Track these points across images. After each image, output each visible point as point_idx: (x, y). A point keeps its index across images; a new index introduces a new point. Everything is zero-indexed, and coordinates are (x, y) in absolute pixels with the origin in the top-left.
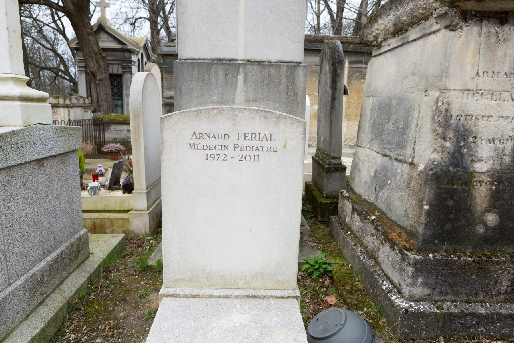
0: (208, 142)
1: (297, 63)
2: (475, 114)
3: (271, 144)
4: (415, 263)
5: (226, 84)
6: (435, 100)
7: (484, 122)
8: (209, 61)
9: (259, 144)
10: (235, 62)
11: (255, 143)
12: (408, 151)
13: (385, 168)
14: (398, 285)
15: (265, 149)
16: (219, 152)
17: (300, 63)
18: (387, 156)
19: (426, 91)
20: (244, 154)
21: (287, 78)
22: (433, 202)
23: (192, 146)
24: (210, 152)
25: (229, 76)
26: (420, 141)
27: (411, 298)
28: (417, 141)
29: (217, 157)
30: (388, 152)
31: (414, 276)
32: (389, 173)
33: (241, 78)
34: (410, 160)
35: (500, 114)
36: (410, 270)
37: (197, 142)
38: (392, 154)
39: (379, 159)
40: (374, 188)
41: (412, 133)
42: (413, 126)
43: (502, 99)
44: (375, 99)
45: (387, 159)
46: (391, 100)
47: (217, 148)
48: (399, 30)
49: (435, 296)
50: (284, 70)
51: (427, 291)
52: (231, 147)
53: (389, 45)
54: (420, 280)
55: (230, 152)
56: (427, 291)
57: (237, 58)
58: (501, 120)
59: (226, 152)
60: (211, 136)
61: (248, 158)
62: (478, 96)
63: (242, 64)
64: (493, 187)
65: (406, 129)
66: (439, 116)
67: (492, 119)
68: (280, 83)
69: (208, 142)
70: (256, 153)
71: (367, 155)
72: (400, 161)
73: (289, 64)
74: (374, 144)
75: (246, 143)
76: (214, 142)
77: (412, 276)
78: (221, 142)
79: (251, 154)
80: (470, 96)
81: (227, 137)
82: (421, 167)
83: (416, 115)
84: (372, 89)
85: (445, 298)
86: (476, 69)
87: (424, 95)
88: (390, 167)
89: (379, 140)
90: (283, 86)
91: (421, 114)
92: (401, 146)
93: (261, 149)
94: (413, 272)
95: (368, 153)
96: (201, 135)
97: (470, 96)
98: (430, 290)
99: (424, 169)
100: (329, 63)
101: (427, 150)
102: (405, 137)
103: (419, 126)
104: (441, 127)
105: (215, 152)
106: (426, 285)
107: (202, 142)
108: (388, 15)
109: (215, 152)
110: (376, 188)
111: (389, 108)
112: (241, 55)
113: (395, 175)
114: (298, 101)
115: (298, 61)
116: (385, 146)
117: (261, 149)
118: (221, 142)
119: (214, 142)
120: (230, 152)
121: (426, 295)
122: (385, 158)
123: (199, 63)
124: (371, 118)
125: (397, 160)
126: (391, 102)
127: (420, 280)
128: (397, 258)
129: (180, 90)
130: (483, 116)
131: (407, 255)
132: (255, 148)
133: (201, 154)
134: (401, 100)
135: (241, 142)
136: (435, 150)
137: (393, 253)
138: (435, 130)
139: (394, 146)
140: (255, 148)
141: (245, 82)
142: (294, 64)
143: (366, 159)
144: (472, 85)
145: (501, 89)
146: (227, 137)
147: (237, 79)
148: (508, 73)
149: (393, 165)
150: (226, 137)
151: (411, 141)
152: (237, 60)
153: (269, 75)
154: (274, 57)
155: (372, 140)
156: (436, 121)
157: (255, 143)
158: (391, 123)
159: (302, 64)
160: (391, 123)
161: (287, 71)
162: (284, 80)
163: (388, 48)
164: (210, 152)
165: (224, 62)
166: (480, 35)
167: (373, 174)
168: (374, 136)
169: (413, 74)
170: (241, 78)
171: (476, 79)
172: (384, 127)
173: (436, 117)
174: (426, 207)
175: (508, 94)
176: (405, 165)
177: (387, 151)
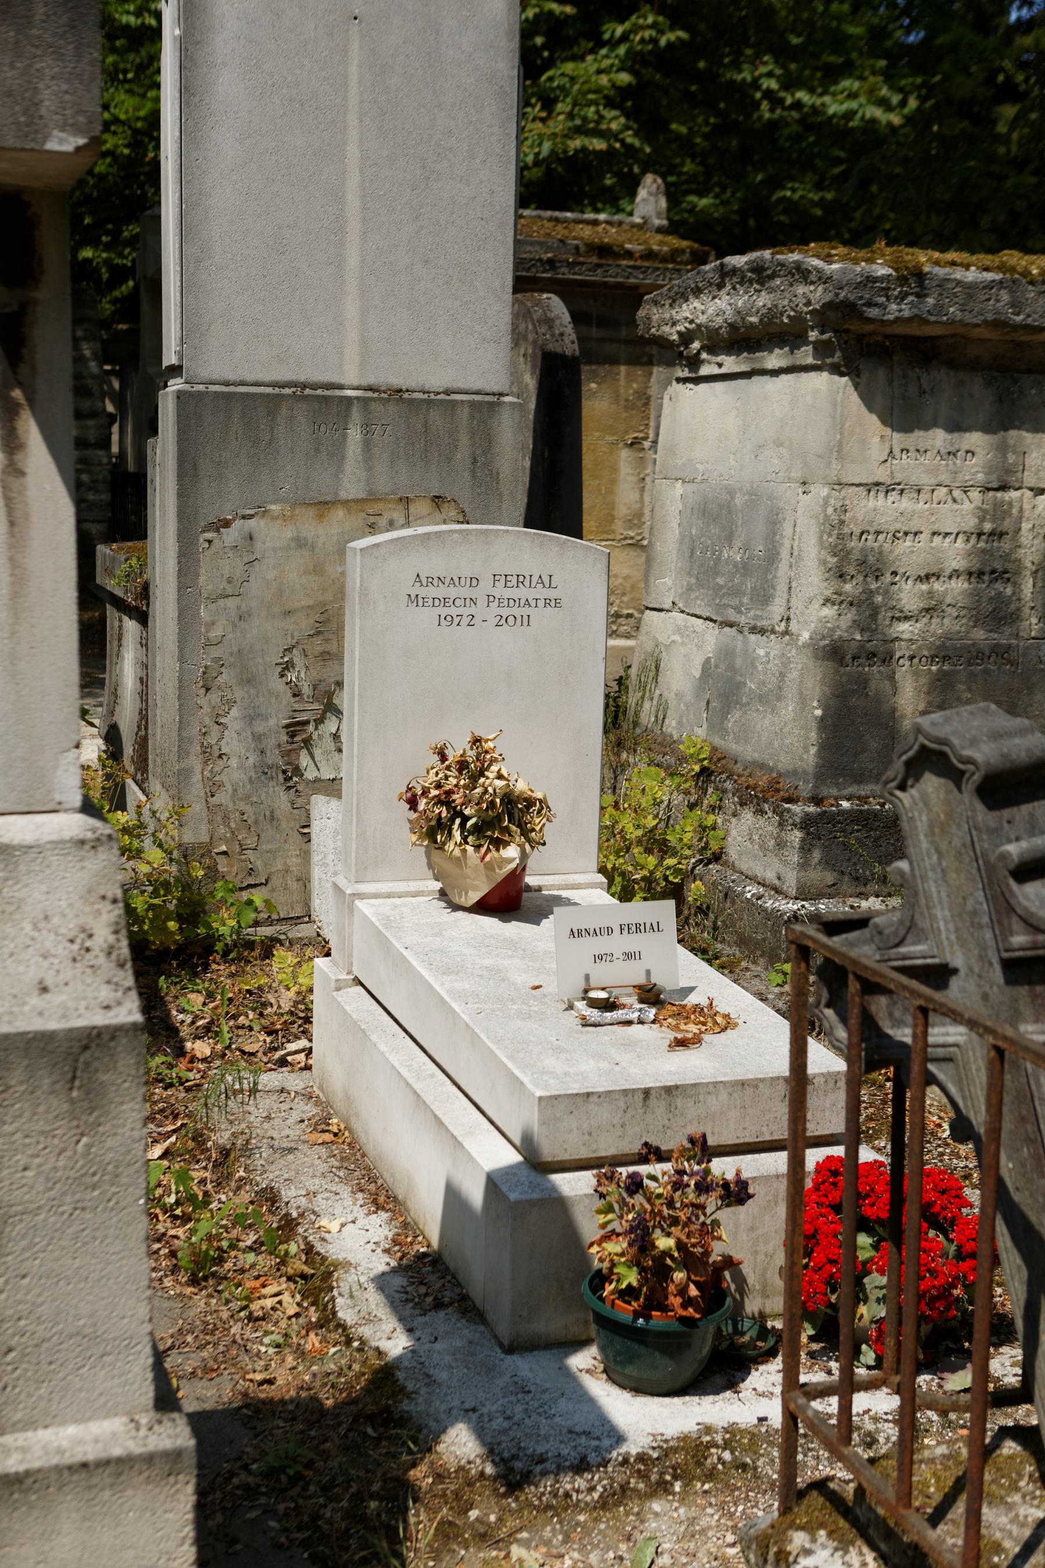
0: (440, 592)
1: (494, 394)
2: (892, 529)
3: (552, 594)
4: (806, 824)
5: (317, 451)
6: (821, 502)
7: (908, 544)
8: (269, 390)
9: (531, 594)
10: (338, 393)
11: (522, 593)
12: (777, 608)
13: (726, 653)
14: (776, 882)
15: (541, 603)
16: (460, 611)
17: (501, 395)
18: (731, 625)
19: (804, 483)
20: (505, 612)
21: (472, 435)
22: (831, 702)
23: (414, 600)
24: (444, 611)
25: (323, 428)
26: (800, 585)
27: (803, 894)
28: (794, 584)
29: (456, 620)
30: (732, 615)
31: (805, 849)
32: (739, 662)
33: (355, 435)
34: (782, 627)
35: (935, 528)
36: (796, 836)
37: (423, 592)
38: (742, 620)
39: (711, 637)
40: (704, 704)
41: (783, 570)
42: (785, 553)
43: (935, 500)
44: (690, 487)
45: (732, 632)
46: (732, 493)
47: (457, 602)
48: (742, 339)
49: (844, 887)
50: (464, 413)
51: (830, 878)
52: (482, 602)
53: (720, 365)
54: (817, 855)
55: (479, 610)
56: (830, 878)
57: (343, 382)
58: (937, 540)
59: (473, 610)
60: (448, 581)
61: (511, 620)
62: (893, 496)
63: (358, 398)
64: (934, 668)
65: (772, 558)
66: (830, 535)
67: (922, 536)
68: (456, 446)
69: (440, 592)
70: (526, 611)
71: (679, 629)
72: (762, 631)
73: (477, 398)
74: (697, 598)
75: (508, 593)
76: (452, 592)
77: (802, 848)
78: (466, 592)
79: (517, 612)
80: (881, 495)
81: (474, 582)
82: (806, 636)
83: (787, 529)
84: (680, 462)
85: (863, 889)
86: (887, 445)
87: (800, 490)
88: (739, 645)
89: (709, 589)
90: (462, 455)
91: (798, 529)
92: (764, 598)
93: (533, 603)
94: (803, 840)
95: (680, 623)
96: (521, 579)
97: (881, 495)
98: (835, 874)
99: (811, 638)
100: (533, 367)
101: (809, 605)
102: (770, 577)
103: (795, 554)
104: (835, 555)
105: (453, 611)
106: (827, 863)
107: (431, 592)
108: (714, 298)
109: (453, 611)
110: (708, 703)
111: (729, 512)
112: (350, 372)
113: (752, 663)
114: (501, 495)
115: (496, 388)
116: (725, 601)
117: (533, 603)
118: (466, 592)
119: (452, 592)
120: (479, 610)
121: (830, 887)
122: (727, 629)
123: (247, 394)
124: (682, 536)
125: (754, 630)
126: (732, 498)
127: (817, 855)
128: (770, 828)
129: (195, 467)
130: (906, 534)
131: (789, 810)
132: (523, 602)
133: (428, 615)
134: (754, 497)
135: (499, 591)
136: (827, 601)
137: (761, 821)
138: (824, 562)
139: (745, 600)
140: (523, 602)
141: (367, 445)
142: (487, 398)
143: (677, 638)
144: (882, 474)
145: (933, 481)
146: (474, 582)
147: (345, 436)
148: (943, 451)
149: (746, 641)
150: (474, 581)
151: (782, 587)
152: (341, 387)
153: (426, 425)
154: (437, 378)
155: (689, 589)
156: (827, 544)
157: (522, 593)
158: (736, 548)
159: (507, 399)
160: (736, 548)
161: (472, 417)
162: (464, 440)
163: (716, 371)
164: (444, 611)
165: (307, 391)
166: (890, 383)
167: (697, 674)
168: (693, 581)
169: (779, 444)
170: (355, 435)
171: (888, 464)
172: (719, 558)
173: (825, 537)
174: (819, 712)
175: (945, 490)
176: (772, 637)
177: (731, 611)
